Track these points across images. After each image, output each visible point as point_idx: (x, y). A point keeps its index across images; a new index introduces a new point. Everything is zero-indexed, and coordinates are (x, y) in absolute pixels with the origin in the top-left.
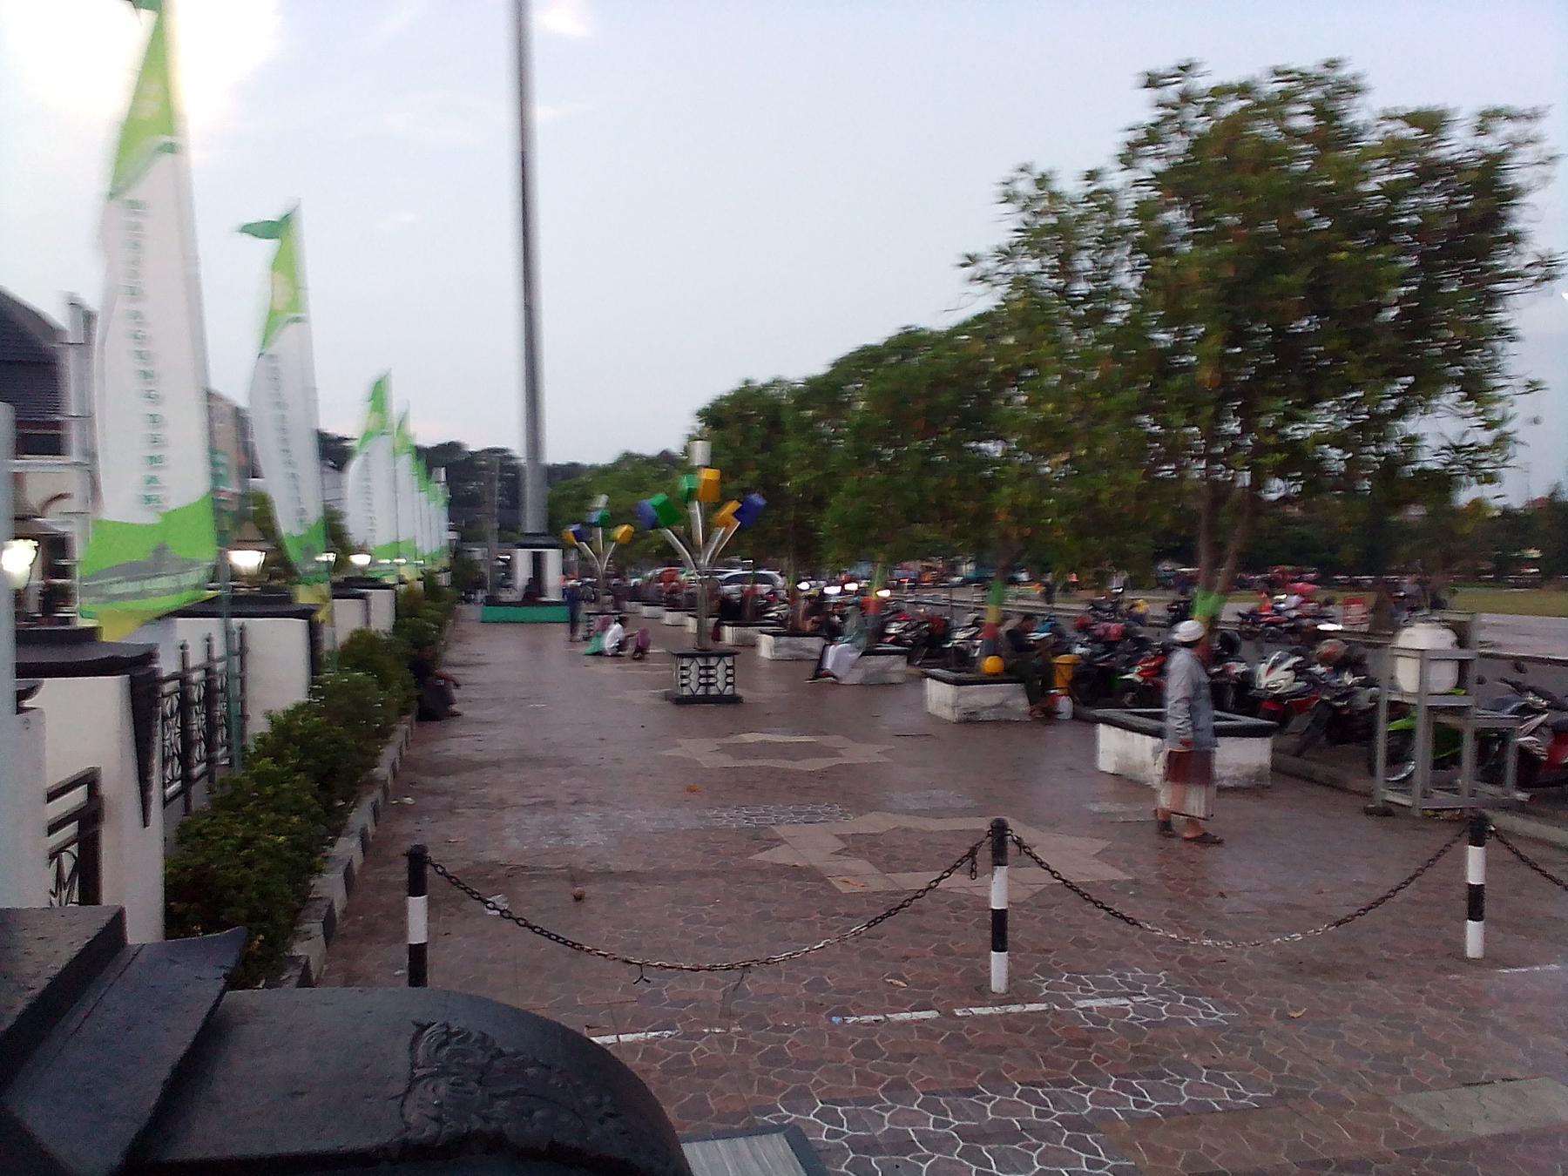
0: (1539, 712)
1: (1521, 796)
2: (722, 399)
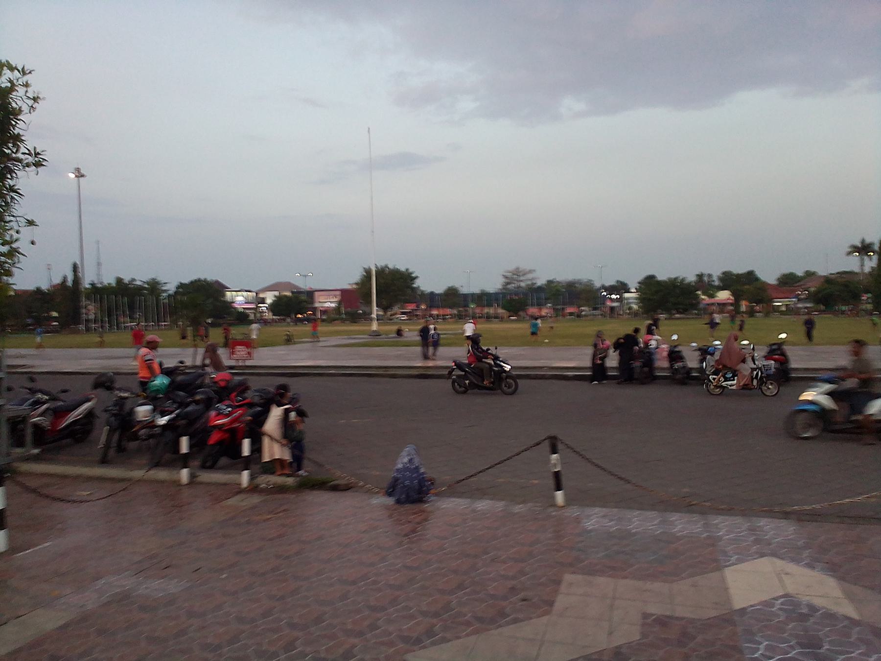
0: (44, 403)
1: (36, 451)
2: (579, 282)
